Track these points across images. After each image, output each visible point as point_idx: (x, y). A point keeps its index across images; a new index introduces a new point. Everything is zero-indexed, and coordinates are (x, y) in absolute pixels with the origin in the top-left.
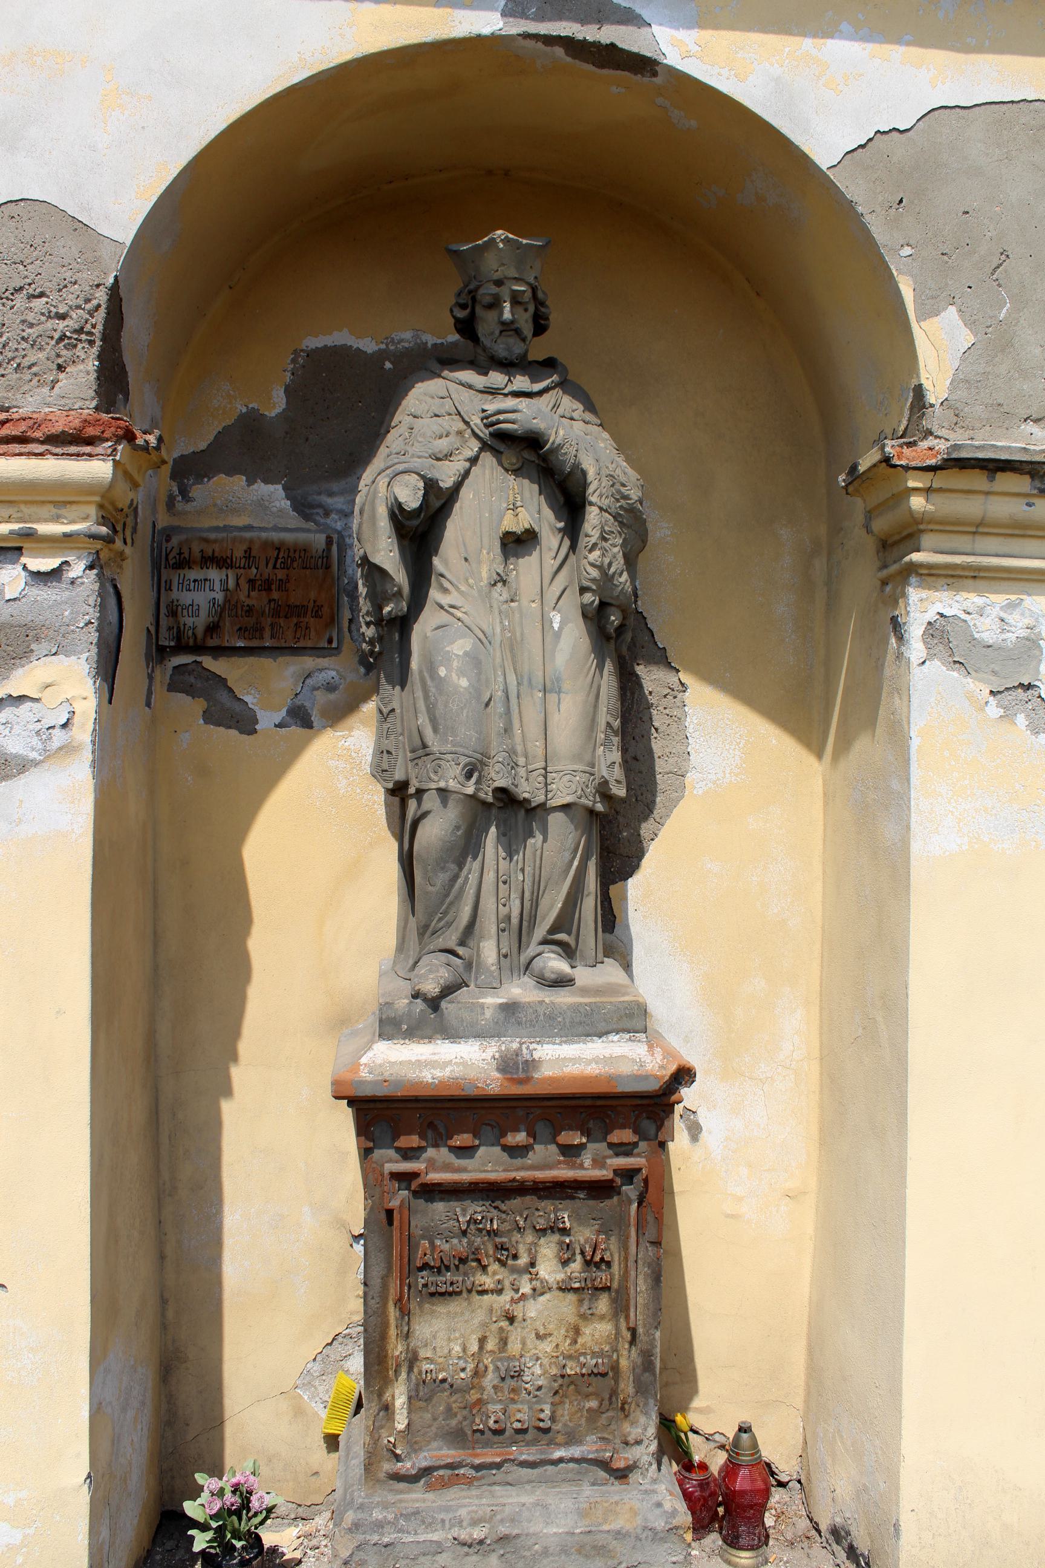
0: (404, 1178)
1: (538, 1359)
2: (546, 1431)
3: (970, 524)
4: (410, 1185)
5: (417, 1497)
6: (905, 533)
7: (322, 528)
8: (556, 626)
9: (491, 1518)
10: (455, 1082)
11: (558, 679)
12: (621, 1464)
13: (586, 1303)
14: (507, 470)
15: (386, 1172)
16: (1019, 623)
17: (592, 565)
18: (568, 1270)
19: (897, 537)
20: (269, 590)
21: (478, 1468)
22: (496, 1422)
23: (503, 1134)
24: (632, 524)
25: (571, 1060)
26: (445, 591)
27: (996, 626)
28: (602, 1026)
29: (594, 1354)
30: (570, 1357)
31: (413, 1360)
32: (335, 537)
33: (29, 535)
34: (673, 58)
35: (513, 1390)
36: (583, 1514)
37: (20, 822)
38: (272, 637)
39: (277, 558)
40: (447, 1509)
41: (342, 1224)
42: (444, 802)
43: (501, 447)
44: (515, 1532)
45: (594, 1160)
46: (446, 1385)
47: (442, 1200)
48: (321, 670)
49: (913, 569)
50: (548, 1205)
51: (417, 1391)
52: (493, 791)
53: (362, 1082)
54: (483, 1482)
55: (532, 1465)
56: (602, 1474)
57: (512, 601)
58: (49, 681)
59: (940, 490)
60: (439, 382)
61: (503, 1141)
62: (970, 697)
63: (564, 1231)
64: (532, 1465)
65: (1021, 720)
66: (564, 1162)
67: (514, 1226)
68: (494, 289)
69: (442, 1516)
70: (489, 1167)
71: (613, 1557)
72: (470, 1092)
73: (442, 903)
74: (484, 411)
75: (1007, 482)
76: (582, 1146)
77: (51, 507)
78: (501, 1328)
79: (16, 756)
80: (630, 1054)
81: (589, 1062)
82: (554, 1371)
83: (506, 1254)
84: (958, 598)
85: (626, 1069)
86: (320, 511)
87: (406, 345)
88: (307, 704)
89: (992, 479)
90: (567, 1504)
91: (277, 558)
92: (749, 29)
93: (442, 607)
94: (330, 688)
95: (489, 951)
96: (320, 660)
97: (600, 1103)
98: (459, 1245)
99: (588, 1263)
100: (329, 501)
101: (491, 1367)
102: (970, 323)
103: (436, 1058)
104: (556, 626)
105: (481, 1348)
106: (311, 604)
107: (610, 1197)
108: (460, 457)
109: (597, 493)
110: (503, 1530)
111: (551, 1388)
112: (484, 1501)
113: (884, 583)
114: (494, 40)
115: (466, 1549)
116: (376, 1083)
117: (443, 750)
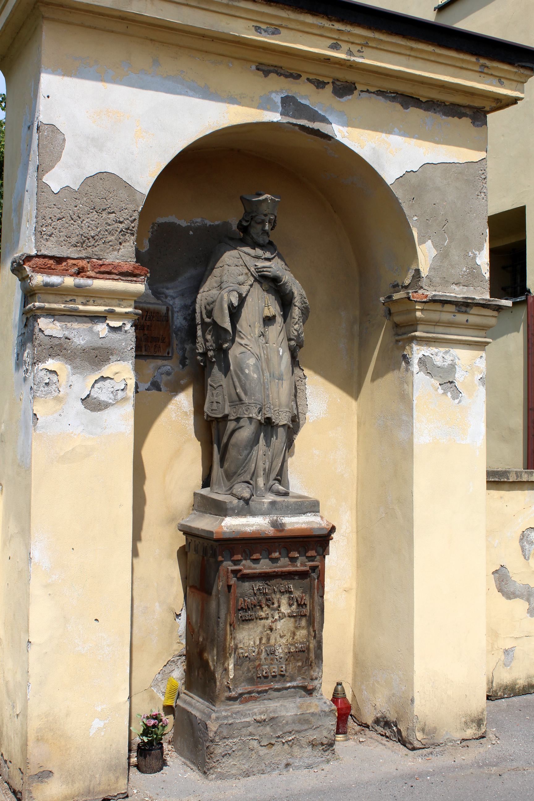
0: (235, 572)
1: (281, 646)
2: (283, 676)
3: (434, 322)
4: (236, 575)
5: (237, 707)
6: (410, 323)
7: (165, 303)
8: (281, 354)
9: (267, 711)
10: (258, 532)
11: (282, 375)
12: (311, 688)
13: (298, 622)
14: (264, 290)
15: (230, 570)
16: (448, 358)
17: (295, 330)
18: (292, 608)
19: (405, 324)
20: (143, 330)
21: (259, 692)
22: (266, 673)
23: (270, 553)
24: (305, 312)
25: (296, 522)
26: (242, 338)
27: (441, 359)
28: (305, 510)
29: (301, 643)
30: (292, 645)
31: (236, 648)
32: (170, 307)
33: (112, 312)
34: (339, 138)
35: (272, 660)
36: (299, 708)
37: (105, 428)
38: (146, 350)
39: (147, 316)
40: (250, 710)
41: (172, 610)
42: (251, 423)
43: (262, 281)
44: (276, 716)
45: (301, 564)
46: (248, 659)
47: (247, 581)
48: (164, 366)
49: (415, 338)
50: (285, 582)
51: (237, 661)
52: (264, 419)
53: (225, 532)
54: (261, 699)
55: (278, 690)
56: (303, 693)
57: (267, 343)
58: (117, 371)
59: (426, 310)
60: (236, 251)
61: (270, 556)
62: (433, 385)
63: (291, 592)
64: (278, 690)
65: (449, 394)
66: (290, 565)
67: (273, 591)
68: (263, 217)
69: (248, 712)
70: (264, 567)
71: (311, 724)
72: (263, 535)
73: (244, 463)
74: (256, 266)
75: (448, 307)
76: (297, 558)
77: (117, 300)
78: (268, 634)
79: (104, 401)
80: (315, 521)
81: (302, 524)
82: (286, 651)
83: (269, 602)
84: (429, 349)
85: (316, 526)
86: (163, 296)
87: (199, 224)
88: (159, 381)
89: (443, 306)
90: (292, 705)
91: (147, 316)
92: (364, 128)
93: (242, 345)
94: (168, 374)
95: (261, 482)
96: (164, 361)
97: (305, 540)
98: (254, 600)
99: (299, 605)
100: (167, 291)
101: (264, 650)
102: (435, 247)
103: (248, 523)
104: (281, 354)
105: (260, 642)
106: (161, 337)
107: (306, 578)
108: (247, 284)
109: (297, 301)
110: (272, 715)
111: (285, 658)
112: (262, 706)
113: (398, 341)
114: (278, 123)
115: (259, 724)
116: (230, 532)
117: (250, 402)
